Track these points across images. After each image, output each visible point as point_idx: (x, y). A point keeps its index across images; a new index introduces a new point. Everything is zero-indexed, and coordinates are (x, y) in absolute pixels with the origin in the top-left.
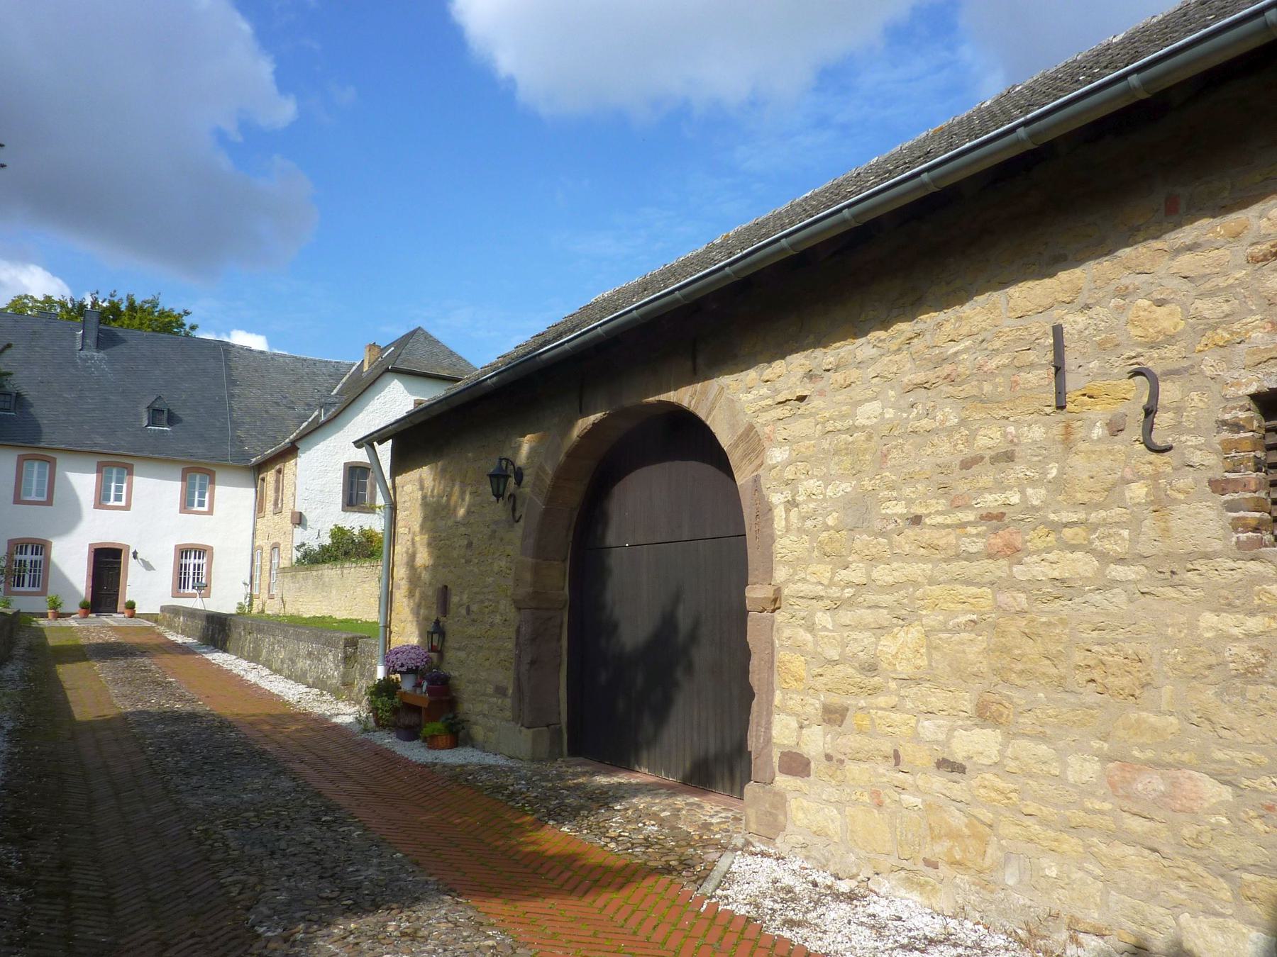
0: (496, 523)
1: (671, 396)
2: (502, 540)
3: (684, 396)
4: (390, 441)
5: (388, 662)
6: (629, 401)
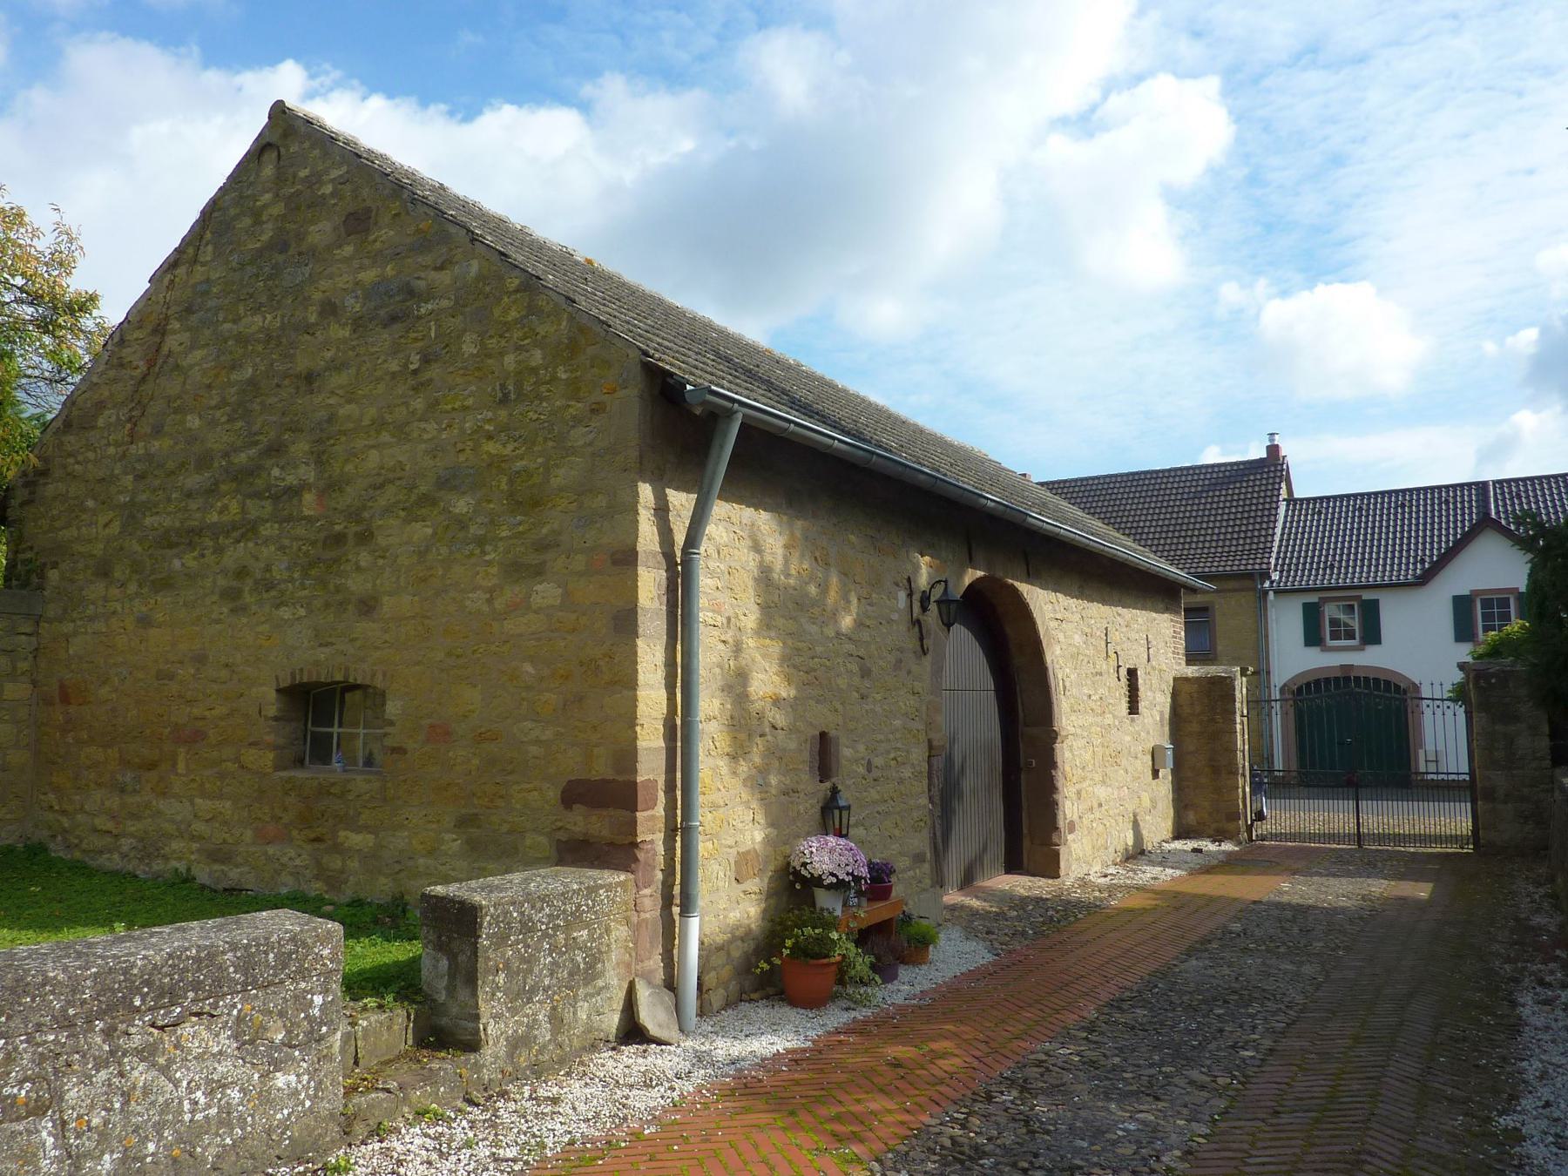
0: (901, 650)
1: (1017, 584)
2: (909, 672)
3: (1024, 588)
4: (668, 491)
5: (97, 871)
6: (999, 574)
